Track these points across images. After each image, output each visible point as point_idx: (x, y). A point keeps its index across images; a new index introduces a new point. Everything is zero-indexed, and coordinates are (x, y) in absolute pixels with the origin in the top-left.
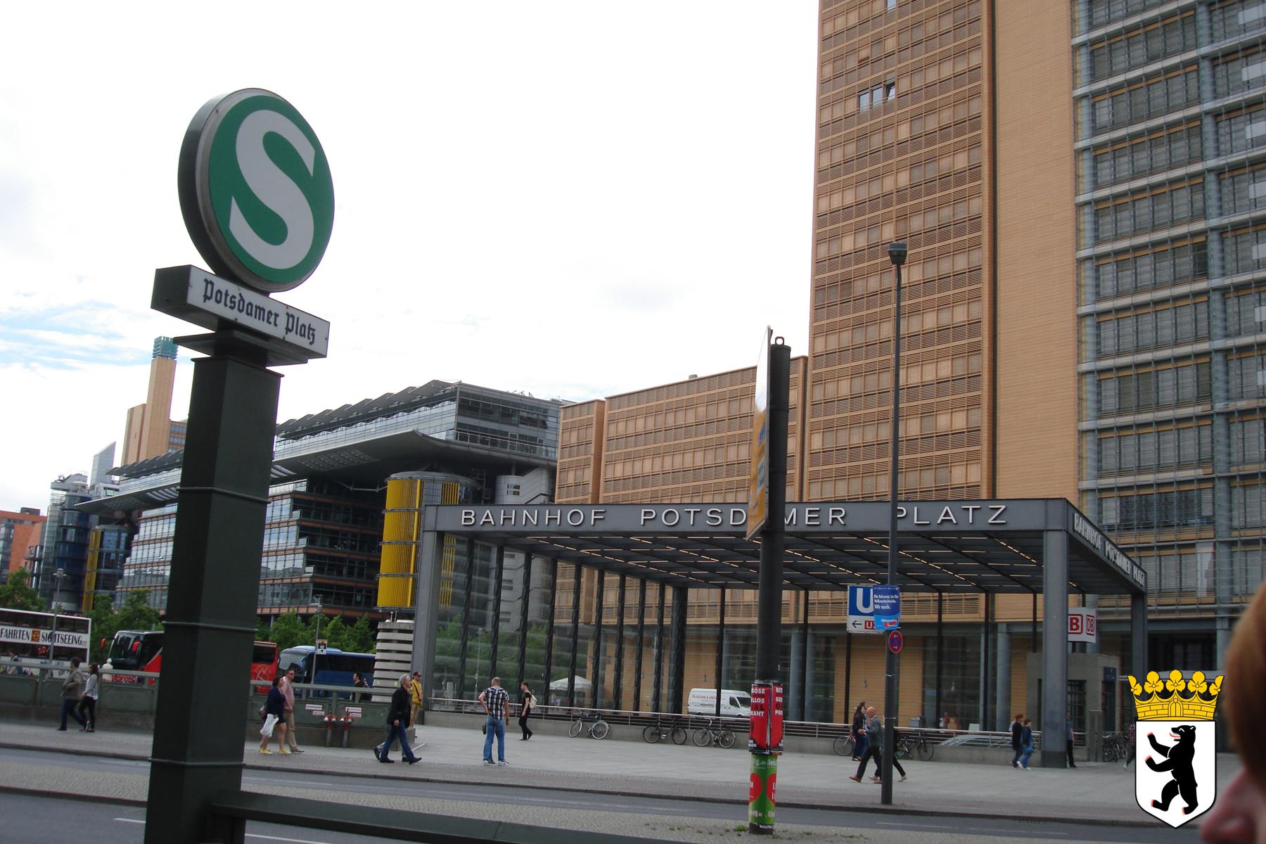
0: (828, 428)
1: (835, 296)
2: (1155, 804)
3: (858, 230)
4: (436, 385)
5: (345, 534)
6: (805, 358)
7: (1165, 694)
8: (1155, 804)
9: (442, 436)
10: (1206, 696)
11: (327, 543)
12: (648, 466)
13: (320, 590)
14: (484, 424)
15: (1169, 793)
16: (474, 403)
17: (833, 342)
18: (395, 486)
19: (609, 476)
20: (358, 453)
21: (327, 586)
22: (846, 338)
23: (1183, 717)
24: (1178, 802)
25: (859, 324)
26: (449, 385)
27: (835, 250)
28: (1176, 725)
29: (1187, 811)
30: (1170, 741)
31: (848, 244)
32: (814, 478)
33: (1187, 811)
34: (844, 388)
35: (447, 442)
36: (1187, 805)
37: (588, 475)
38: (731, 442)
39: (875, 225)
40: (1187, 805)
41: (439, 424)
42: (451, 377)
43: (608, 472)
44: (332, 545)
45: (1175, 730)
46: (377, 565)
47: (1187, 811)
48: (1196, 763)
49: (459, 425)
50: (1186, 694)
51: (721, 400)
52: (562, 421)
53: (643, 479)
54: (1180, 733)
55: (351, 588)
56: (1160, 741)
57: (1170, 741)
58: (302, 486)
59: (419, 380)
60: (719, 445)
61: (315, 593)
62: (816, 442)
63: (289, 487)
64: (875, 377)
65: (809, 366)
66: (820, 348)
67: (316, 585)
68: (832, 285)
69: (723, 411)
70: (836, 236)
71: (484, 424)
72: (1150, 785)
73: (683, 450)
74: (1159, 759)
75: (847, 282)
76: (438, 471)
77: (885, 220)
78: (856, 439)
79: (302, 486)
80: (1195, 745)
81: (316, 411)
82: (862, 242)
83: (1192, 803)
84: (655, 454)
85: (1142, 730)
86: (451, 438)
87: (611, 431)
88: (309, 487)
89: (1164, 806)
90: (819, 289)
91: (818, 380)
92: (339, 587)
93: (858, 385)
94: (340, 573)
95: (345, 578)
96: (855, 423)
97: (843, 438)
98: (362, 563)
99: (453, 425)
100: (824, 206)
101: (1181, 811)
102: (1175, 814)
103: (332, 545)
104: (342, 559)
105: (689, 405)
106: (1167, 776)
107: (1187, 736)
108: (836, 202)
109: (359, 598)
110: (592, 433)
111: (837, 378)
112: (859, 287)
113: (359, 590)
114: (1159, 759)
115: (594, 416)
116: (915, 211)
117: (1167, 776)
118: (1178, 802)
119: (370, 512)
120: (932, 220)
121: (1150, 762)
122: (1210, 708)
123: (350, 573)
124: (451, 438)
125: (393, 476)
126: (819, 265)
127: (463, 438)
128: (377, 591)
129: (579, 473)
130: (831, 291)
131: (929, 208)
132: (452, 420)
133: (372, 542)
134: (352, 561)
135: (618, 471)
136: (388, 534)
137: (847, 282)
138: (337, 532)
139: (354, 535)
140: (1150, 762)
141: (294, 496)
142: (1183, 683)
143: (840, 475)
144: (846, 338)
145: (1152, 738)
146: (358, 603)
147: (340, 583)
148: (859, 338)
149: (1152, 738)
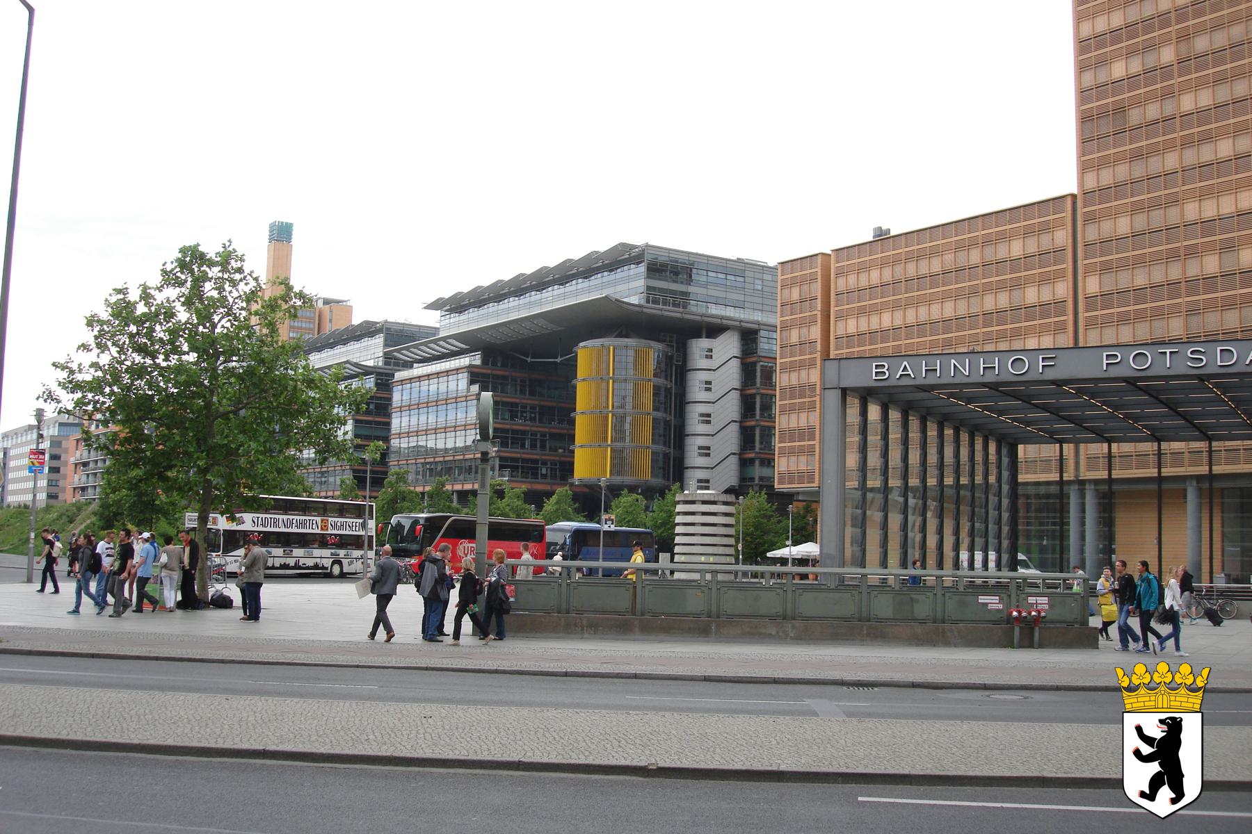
0: (1106, 268)
1: (1106, 127)
2: (1143, 795)
3: (1130, 53)
4: (624, 247)
5: (524, 407)
6: (1074, 196)
7: (1151, 687)
8: (1143, 795)
9: (634, 300)
10: (1192, 689)
11: (507, 415)
12: (886, 320)
13: (506, 464)
14: (673, 286)
15: (1156, 783)
16: (668, 269)
17: (1107, 177)
18: (585, 352)
19: (841, 332)
20: (542, 322)
21: (513, 459)
22: (1122, 172)
23: (1170, 708)
24: (1165, 793)
25: (1137, 155)
26: (636, 247)
27: (1102, 77)
28: (1163, 716)
29: (1174, 801)
30: (1157, 732)
31: (1118, 70)
32: (1091, 323)
33: (1174, 801)
34: (1123, 225)
35: (640, 306)
36: (1173, 796)
37: (816, 332)
38: (988, 289)
39: (1150, 47)
40: (1173, 796)
41: (630, 289)
42: (637, 239)
43: (838, 329)
44: (512, 418)
45: (1162, 721)
46: (572, 438)
47: (1174, 801)
48: (1183, 754)
49: (649, 288)
50: (1173, 687)
51: (972, 244)
52: (780, 278)
53: (884, 334)
54: (1168, 724)
55: (536, 461)
56: (1147, 732)
57: (1157, 732)
58: (477, 360)
59: (603, 245)
60: (974, 292)
61: (501, 467)
62: (814, 418)
63: (464, 361)
64: (1162, 211)
65: (1079, 203)
66: (1091, 183)
67: (501, 459)
68: (1103, 114)
69: (975, 257)
70: (1103, 62)
71: (673, 286)
72: (1138, 776)
73: (929, 301)
74: (1146, 750)
75: (1120, 110)
76: (627, 337)
77: (1165, 41)
78: (1141, 279)
79: (477, 360)
80: (1182, 736)
81: (486, 282)
82: (1136, 66)
83: (1179, 794)
84: (896, 306)
85: (1130, 721)
86: (643, 302)
87: (840, 284)
88: (485, 361)
89: (1151, 796)
90: (1085, 119)
91: (1090, 219)
92: (524, 461)
93: (1140, 222)
94: (523, 446)
95: (538, 451)
96: (1139, 262)
97: (1124, 280)
98: (543, 435)
99: (643, 289)
100: (1086, 29)
101: (1168, 802)
102: (1163, 804)
103: (512, 418)
104: (524, 432)
105: (934, 252)
106: (1155, 767)
107: (1174, 727)
108: (1101, 24)
109: (544, 471)
110: (817, 289)
111: (1114, 214)
112: (1135, 117)
113: (544, 463)
114: (1146, 750)
115: (819, 270)
116: (1200, 30)
117: (1155, 767)
118: (1165, 793)
119: (561, 378)
120: (1221, 39)
121: (1137, 753)
122: (1196, 700)
123: (533, 446)
124: (643, 302)
125: (581, 344)
126: (1083, 94)
127: (656, 302)
128: (573, 463)
129: (804, 330)
130: (1103, 121)
131: (1217, 26)
132: (640, 283)
133: (566, 414)
134: (534, 434)
135: (852, 326)
136: (581, 404)
137: (1120, 110)
138: (516, 405)
139: (533, 408)
140: (1137, 753)
141: (471, 369)
142: (1169, 676)
143: (1123, 319)
144: (1122, 172)
145: (1139, 729)
146: (544, 476)
147: (525, 456)
148: (1139, 170)
149: (1139, 729)
